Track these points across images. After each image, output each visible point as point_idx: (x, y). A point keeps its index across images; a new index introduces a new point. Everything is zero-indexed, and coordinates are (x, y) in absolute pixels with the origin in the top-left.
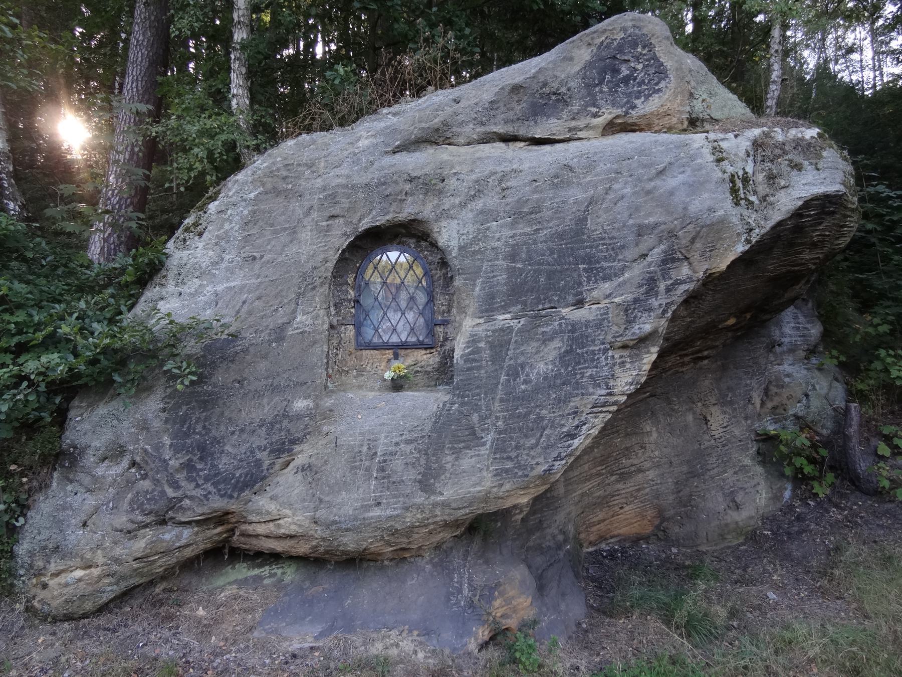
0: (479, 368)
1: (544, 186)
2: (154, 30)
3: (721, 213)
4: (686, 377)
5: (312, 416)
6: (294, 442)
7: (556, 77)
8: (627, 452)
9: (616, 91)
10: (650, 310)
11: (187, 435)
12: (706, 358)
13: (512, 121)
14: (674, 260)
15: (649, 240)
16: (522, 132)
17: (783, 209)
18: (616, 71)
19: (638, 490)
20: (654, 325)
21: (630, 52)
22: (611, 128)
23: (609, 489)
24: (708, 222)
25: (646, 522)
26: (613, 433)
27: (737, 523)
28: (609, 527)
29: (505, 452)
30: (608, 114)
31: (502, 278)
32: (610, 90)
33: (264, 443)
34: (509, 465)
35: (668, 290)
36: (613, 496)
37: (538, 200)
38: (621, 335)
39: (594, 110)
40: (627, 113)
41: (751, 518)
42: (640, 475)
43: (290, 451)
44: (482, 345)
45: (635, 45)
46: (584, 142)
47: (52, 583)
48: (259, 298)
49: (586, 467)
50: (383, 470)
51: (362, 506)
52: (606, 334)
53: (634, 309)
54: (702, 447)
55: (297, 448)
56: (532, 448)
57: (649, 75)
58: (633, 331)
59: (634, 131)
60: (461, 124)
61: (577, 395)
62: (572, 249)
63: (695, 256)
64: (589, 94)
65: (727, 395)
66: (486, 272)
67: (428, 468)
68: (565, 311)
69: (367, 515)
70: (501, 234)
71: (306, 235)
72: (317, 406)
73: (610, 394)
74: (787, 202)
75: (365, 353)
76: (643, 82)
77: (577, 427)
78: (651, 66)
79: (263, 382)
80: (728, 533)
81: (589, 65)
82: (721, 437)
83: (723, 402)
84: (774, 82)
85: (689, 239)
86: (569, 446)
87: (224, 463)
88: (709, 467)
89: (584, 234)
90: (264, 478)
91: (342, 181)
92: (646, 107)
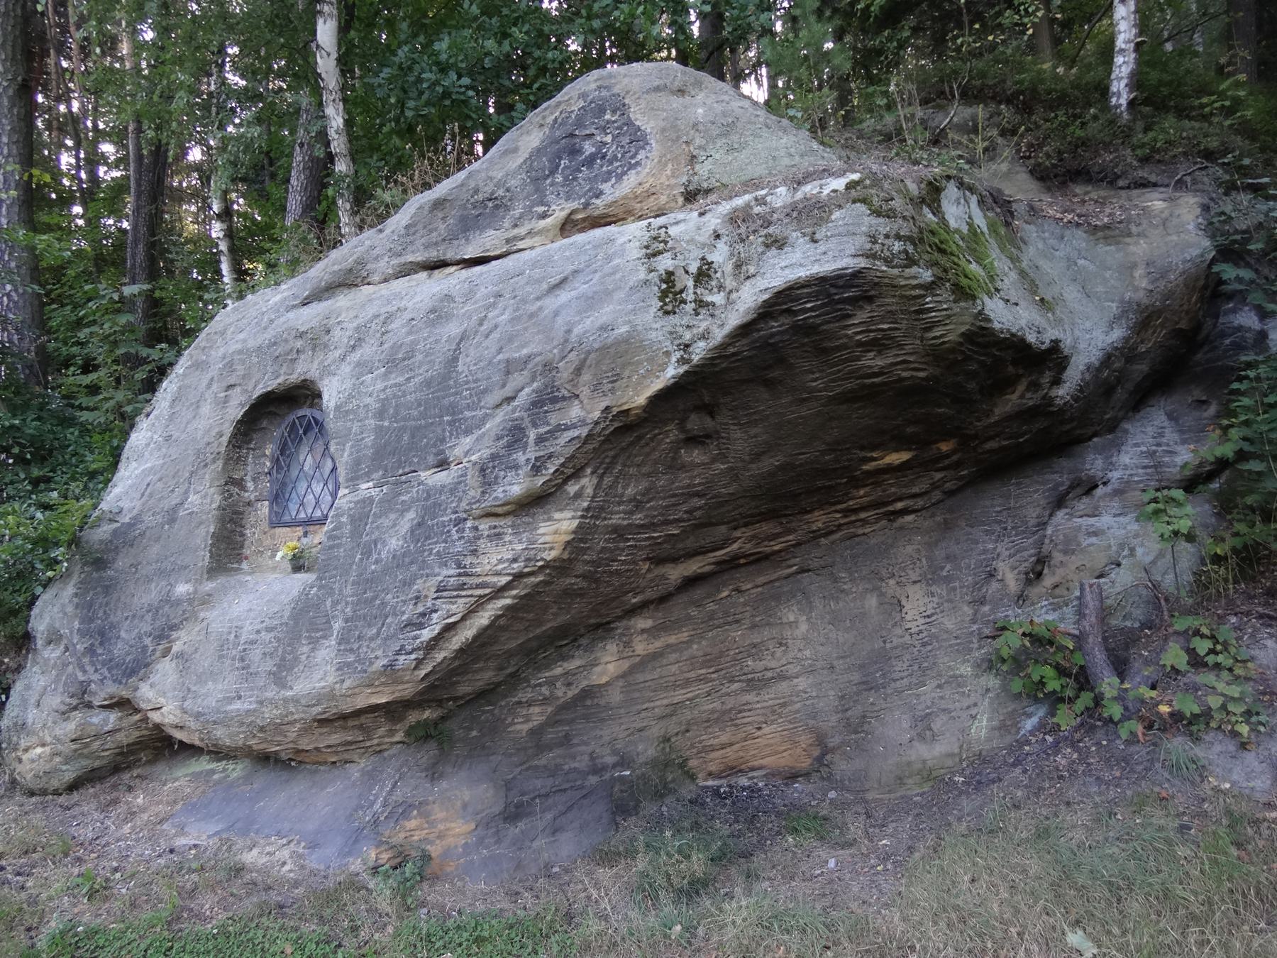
0: (339, 546)
1: (420, 325)
2: (307, 173)
3: (623, 329)
4: (873, 541)
5: (190, 601)
6: (174, 627)
7: (491, 179)
8: (755, 650)
9: (575, 179)
10: (516, 467)
11: (91, 620)
12: (905, 512)
13: (436, 244)
14: (554, 400)
15: (517, 379)
16: (450, 255)
17: (742, 309)
18: (574, 152)
19: (784, 705)
20: (525, 485)
21: (594, 123)
22: (568, 226)
23: (730, 702)
24: (596, 346)
25: (799, 750)
26: (729, 623)
27: (924, 761)
28: (741, 754)
29: (348, 642)
30: (559, 212)
31: (369, 439)
32: (566, 179)
33: (149, 628)
34: (351, 658)
35: (540, 440)
36: (740, 712)
37: (412, 342)
38: (478, 501)
39: (541, 209)
40: (586, 205)
41: (951, 755)
42: (784, 684)
43: (168, 637)
44: (344, 519)
45: (602, 111)
46: (527, 252)
47: (24, 758)
48: (160, 480)
49: (674, 668)
50: (242, 660)
51: (224, 698)
52: (460, 500)
53: (494, 467)
54: (888, 646)
55: (174, 635)
56: (372, 639)
57: (622, 147)
58: (495, 494)
59: (609, 224)
60: (376, 259)
61: (422, 576)
62: (438, 398)
63: (585, 392)
64: (537, 190)
65: (942, 568)
66: (356, 435)
67: (283, 659)
68: (423, 475)
69: (230, 708)
70: (375, 384)
71: (206, 409)
72: (196, 591)
73: (466, 575)
74: (749, 298)
75: (278, 530)
76: (615, 158)
77: (423, 615)
78: (624, 135)
79: (154, 566)
80: (910, 776)
81: (538, 152)
82: (921, 632)
83: (932, 577)
84: (1122, 51)
85: (571, 370)
86: (416, 638)
87: (119, 649)
88: (895, 676)
89: (450, 379)
90: (147, 665)
91: (239, 346)
92: (612, 192)
